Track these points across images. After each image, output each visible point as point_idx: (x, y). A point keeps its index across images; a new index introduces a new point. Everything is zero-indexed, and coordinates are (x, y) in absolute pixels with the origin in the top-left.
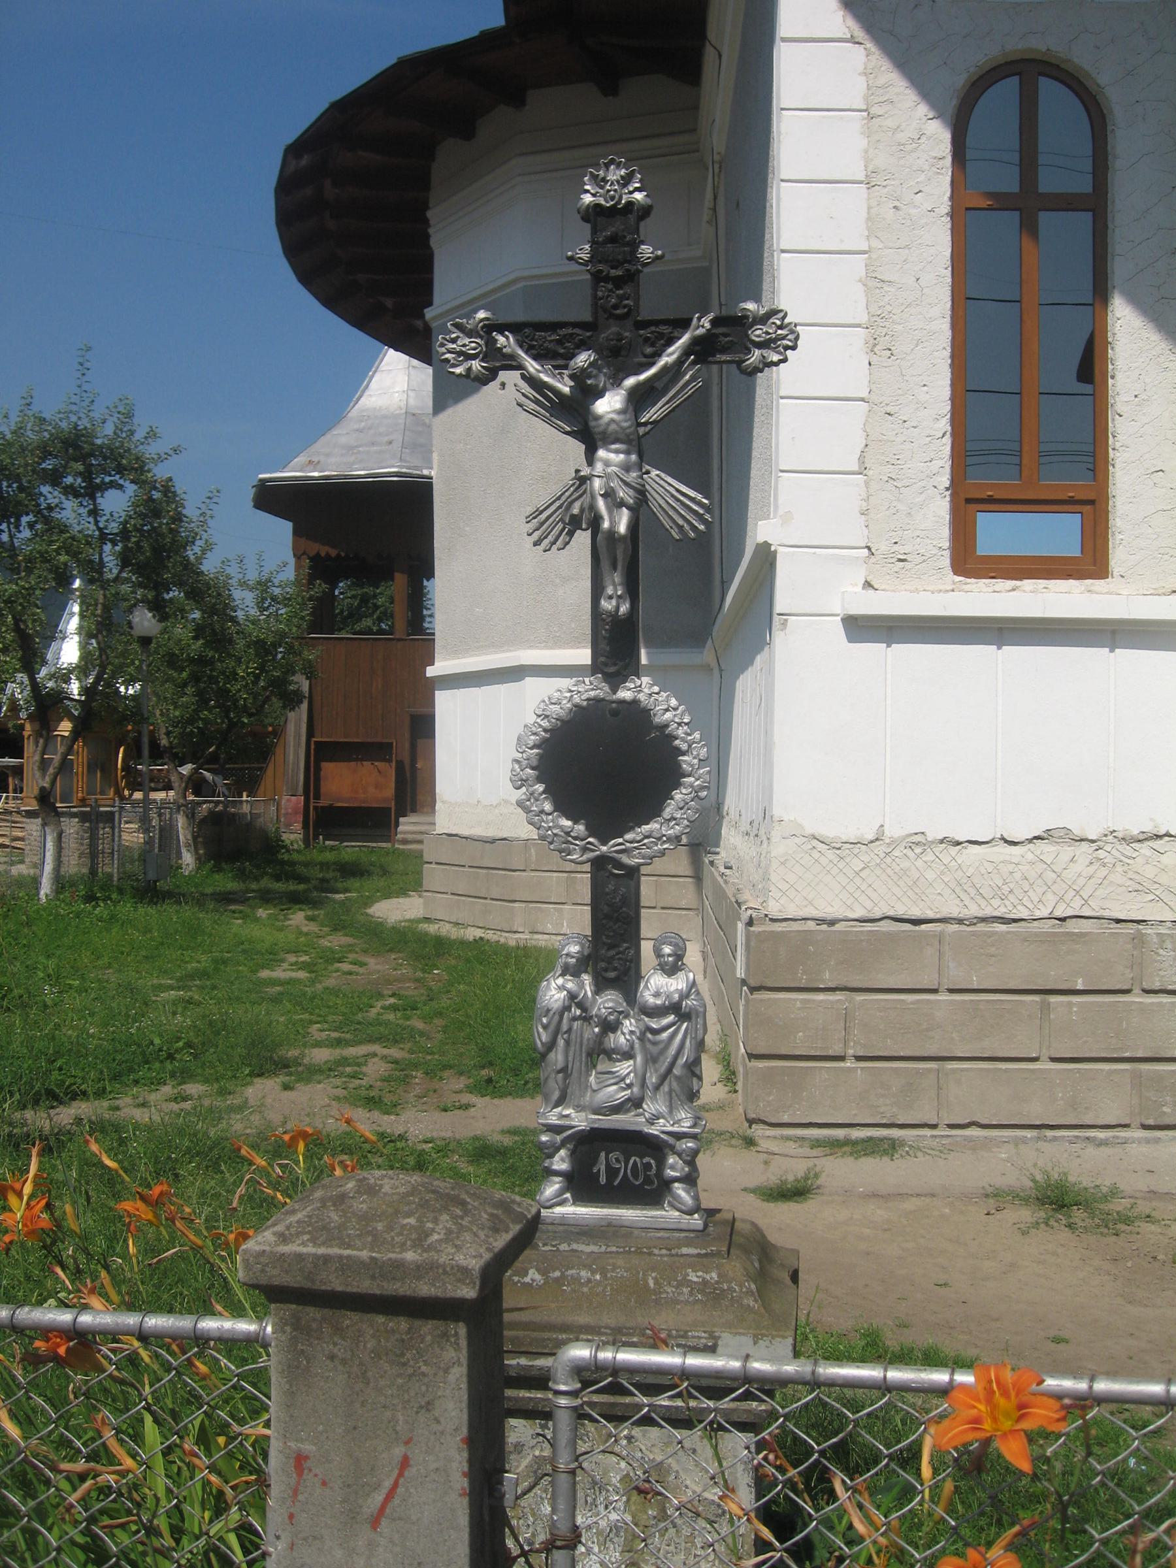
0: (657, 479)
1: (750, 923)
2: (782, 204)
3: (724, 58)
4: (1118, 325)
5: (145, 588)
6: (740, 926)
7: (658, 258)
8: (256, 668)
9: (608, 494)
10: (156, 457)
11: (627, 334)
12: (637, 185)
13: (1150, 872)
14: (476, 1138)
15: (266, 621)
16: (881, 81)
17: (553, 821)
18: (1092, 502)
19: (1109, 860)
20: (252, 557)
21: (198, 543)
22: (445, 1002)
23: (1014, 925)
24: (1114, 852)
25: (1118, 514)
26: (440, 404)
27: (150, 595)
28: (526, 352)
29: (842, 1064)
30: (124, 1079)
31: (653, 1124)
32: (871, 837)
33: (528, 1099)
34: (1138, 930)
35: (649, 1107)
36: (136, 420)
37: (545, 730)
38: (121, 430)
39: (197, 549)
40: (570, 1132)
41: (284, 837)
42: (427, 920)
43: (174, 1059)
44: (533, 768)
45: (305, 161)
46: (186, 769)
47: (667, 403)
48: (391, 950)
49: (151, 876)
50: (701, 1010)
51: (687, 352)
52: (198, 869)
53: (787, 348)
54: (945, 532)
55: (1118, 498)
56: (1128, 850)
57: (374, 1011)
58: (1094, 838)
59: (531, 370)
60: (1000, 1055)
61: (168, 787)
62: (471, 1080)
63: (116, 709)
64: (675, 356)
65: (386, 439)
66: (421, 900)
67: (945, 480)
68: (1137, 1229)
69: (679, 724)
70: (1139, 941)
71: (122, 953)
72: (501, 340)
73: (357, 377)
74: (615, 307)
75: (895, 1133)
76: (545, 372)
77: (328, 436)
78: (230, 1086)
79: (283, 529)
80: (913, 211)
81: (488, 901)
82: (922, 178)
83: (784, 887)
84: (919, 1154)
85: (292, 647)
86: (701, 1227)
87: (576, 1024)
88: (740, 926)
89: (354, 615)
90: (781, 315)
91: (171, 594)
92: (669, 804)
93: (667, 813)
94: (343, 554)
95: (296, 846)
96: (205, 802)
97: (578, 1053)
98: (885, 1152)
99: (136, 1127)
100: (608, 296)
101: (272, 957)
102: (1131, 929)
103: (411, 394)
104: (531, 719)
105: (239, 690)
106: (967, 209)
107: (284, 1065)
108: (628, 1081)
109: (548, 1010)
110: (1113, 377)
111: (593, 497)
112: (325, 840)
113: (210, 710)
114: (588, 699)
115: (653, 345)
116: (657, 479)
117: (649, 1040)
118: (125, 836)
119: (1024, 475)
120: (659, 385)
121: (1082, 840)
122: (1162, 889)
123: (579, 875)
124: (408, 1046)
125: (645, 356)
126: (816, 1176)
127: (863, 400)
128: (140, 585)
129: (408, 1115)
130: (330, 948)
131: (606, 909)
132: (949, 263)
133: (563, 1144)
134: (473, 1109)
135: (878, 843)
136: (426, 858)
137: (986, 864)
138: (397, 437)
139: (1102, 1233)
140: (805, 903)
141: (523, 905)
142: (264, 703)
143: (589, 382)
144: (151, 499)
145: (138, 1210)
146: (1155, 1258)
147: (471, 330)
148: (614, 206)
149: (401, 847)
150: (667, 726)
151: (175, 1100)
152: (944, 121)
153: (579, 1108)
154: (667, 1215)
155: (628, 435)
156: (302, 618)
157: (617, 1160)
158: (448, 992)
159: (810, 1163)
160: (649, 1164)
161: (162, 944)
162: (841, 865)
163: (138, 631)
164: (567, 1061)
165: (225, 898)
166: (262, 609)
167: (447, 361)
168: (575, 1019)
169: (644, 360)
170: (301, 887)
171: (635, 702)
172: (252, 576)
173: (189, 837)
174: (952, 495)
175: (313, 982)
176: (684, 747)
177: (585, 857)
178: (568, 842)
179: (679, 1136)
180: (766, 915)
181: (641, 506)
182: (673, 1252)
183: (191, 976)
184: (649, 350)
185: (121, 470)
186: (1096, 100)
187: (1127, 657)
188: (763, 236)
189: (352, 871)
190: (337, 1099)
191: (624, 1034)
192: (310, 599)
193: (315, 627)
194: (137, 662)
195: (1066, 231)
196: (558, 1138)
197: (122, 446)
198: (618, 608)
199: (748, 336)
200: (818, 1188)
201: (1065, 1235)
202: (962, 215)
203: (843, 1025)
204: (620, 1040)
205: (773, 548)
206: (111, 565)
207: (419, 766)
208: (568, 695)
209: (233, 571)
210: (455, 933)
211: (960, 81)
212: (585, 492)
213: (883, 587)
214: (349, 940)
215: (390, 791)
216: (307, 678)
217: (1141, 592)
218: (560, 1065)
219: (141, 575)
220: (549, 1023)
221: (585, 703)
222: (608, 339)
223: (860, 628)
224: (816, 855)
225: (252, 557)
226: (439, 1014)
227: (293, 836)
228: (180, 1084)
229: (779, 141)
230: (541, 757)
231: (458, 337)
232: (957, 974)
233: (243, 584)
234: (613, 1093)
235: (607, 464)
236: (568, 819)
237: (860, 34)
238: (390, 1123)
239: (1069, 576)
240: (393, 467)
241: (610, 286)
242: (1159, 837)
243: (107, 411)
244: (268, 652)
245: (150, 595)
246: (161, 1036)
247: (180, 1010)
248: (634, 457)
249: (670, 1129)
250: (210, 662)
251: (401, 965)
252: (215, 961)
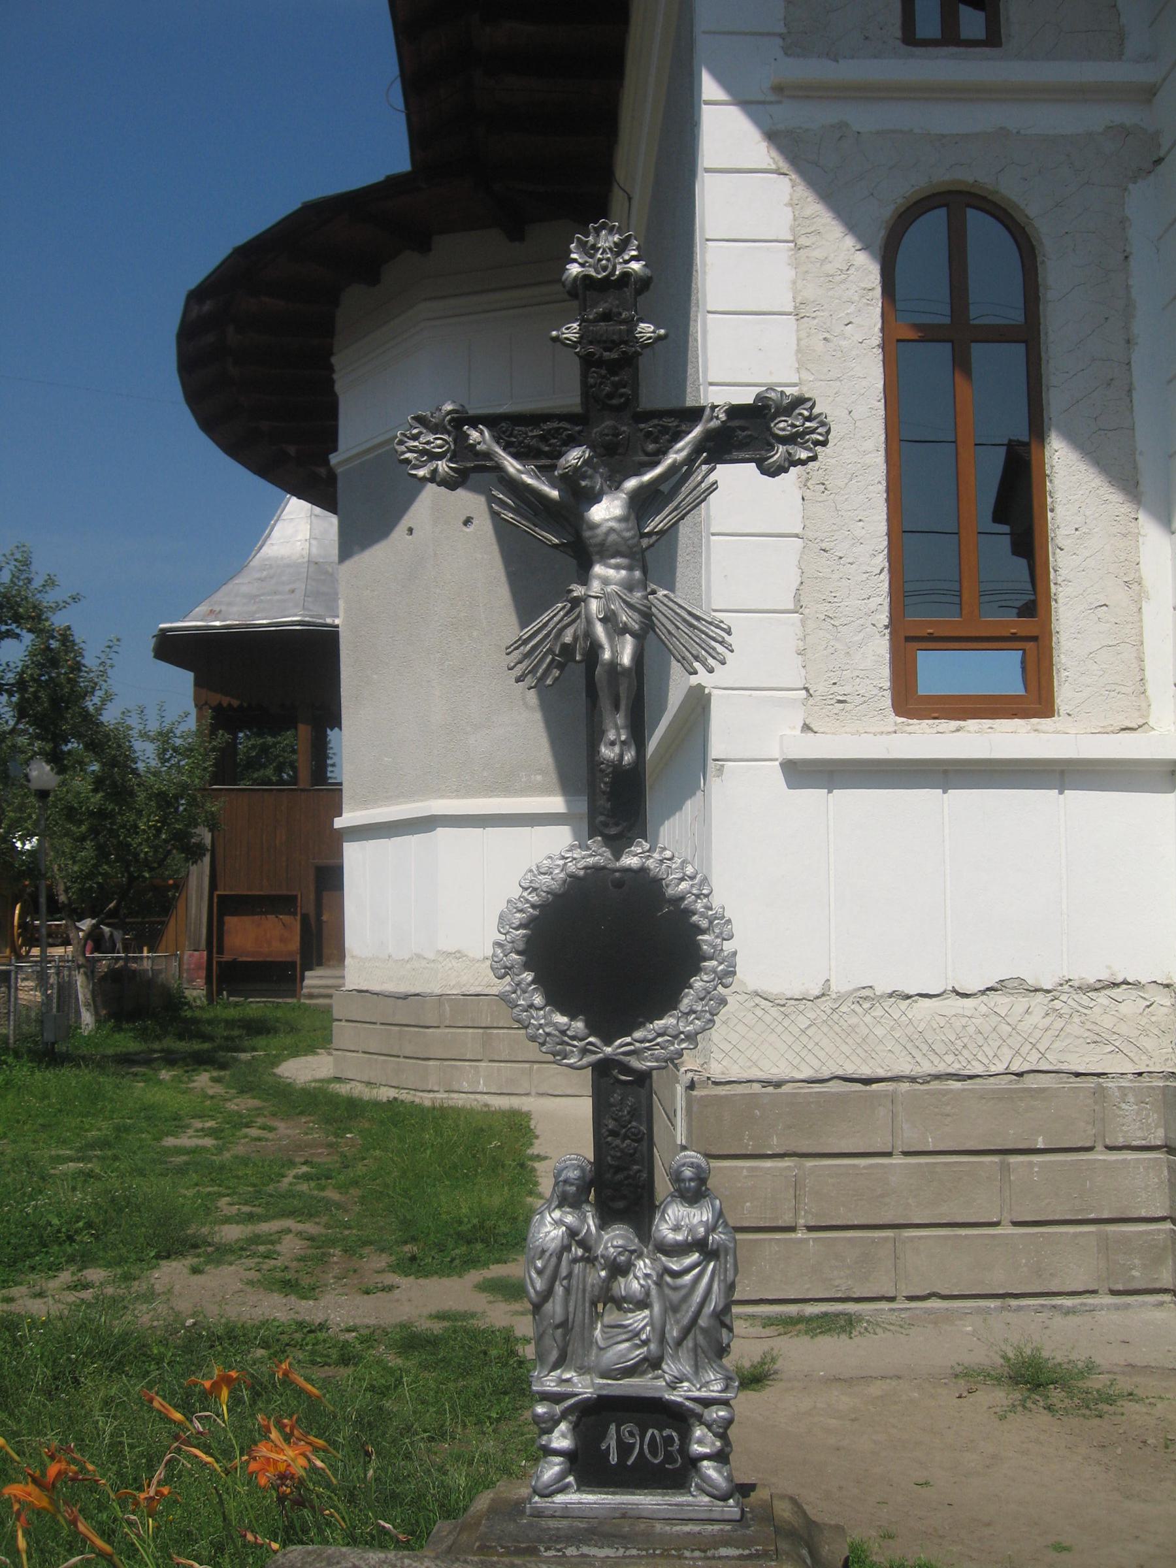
0: (666, 600)
1: (692, 1086)
2: (710, 337)
3: (635, 203)
4: (1056, 457)
5: (42, 740)
6: (680, 1089)
7: (660, 338)
8: (157, 821)
9: (609, 619)
10: (53, 605)
11: (624, 428)
12: (634, 253)
13: (1108, 1022)
14: (403, 1326)
15: (168, 773)
16: (808, 212)
17: (544, 1017)
18: (1035, 639)
19: (1065, 1010)
20: (148, 706)
21: (98, 693)
22: (360, 1169)
23: (969, 1081)
24: (1070, 1002)
25: (1063, 651)
26: (345, 553)
27: (48, 747)
28: (504, 450)
29: (793, 1235)
30: (19, 1265)
31: (674, 1388)
32: (817, 992)
33: (455, 1278)
34: (1099, 1084)
35: (670, 1368)
36: (33, 568)
37: (533, 906)
38: (18, 578)
39: (96, 700)
40: (572, 1401)
41: (187, 993)
42: (338, 1079)
43: (74, 1241)
44: (519, 953)
45: (207, 307)
46: (86, 924)
47: (675, 509)
48: (302, 1113)
49: (49, 1036)
50: (731, 1245)
51: (697, 449)
52: (98, 1028)
53: (817, 443)
54: (886, 672)
55: (1061, 633)
56: (1084, 1000)
57: (286, 1180)
58: (1049, 987)
59: (511, 470)
60: (959, 1220)
61: (66, 942)
62: (393, 1258)
63: (12, 865)
64: (684, 453)
65: (288, 588)
66: (331, 1058)
67: (883, 618)
68: (1120, 1410)
69: (698, 896)
70: (1100, 1094)
71: (18, 1122)
72: (474, 435)
73: (258, 527)
74: (610, 396)
75: (850, 1307)
76: (527, 473)
77: (230, 586)
78: (135, 1270)
79: (182, 681)
80: (844, 343)
81: (401, 1060)
82: (852, 309)
83: (727, 1047)
84: (879, 1330)
85: (195, 799)
86: (738, 1517)
87: (577, 1268)
88: (680, 1089)
89: (252, 764)
90: (809, 404)
91: (70, 746)
92: (687, 995)
93: (685, 1004)
94: (245, 705)
95: (198, 1003)
96: (105, 958)
97: (580, 1302)
98: (843, 1329)
99: (33, 1325)
100: (601, 384)
101: (177, 1123)
102: (1091, 1083)
103: (314, 542)
104: (517, 892)
105: (141, 844)
106: (898, 341)
107: (194, 1245)
108: (644, 1337)
109: (543, 1252)
110: (1052, 510)
111: (589, 622)
112: (229, 995)
113: (108, 863)
114: (586, 868)
115: (656, 441)
116: (666, 600)
117: (668, 1285)
118: (21, 995)
119: (964, 612)
120: (665, 488)
121: (1036, 990)
122: (1121, 1039)
123: (495, 1031)
124: (324, 1219)
125: (647, 454)
126: (773, 1360)
127: (797, 536)
128: (38, 737)
129: (328, 1299)
130: (237, 1112)
131: (611, 1124)
132: (882, 395)
133: (564, 1415)
134: (397, 1291)
135: (824, 999)
136: (336, 1015)
137: (938, 1018)
138: (301, 586)
139: (1084, 1416)
140: (749, 1064)
141: (438, 1063)
142: (166, 857)
143: (583, 483)
144: (48, 648)
145: (30, 1495)
146: (1145, 1442)
147: (436, 425)
148: (607, 278)
149: (307, 1001)
150: (683, 898)
151: (75, 1288)
152: (873, 255)
153: (582, 1370)
154: (695, 1500)
155: (630, 548)
156: (205, 769)
157: (631, 1434)
158: (364, 1159)
159: (765, 1345)
160: (671, 1437)
161: (60, 1111)
162: (786, 1023)
163: (34, 785)
164: (567, 1313)
165: (126, 1059)
166: (164, 761)
167: (407, 461)
168: (575, 1260)
169: (646, 458)
170: (208, 1047)
171: (643, 870)
172: (153, 727)
173: (89, 996)
174: (891, 633)
175: (220, 1150)
176: (704, 924)
177: (585, 1061)
178: (563, 1043)
179: (707, 1403)
180: (709, 1078)
181: (647, 633)
182: (709, 1553)
183: (92, 1146)
184: (651, 447)
185: (17, 619)
186: (1025, 232)
187: (1076, 798)
188: (686, 371)
189: (258, 1028)
190: (251, 1283)
191: (637, 1278)
192: (214, 749)
193: (216, 778)
194: (34, 816)
195: (998, 362)
196: (558, 1409)
197: (19, 594)
198: (621, 756)
199: (769, 429)
200: (776, 1372)
201: (1045, 1418)
202: (894, 347)
203: (792, 1191)
204: (633, 1285)
205: (707, 691)
206: (7, 716)
207: (324, 918)
208: (561, 862)
209: (133, 721)
210: (367, 1094)
211: (887, 212)
212: (578, 616)
213: (822, 730)
214: (257, 1103)
215: (295, 944)
216: (211, 830)
217: (1089, 730)
218: (559, 1318)
219: (39, 727)
220: (545, 1267)
221: (582, 873)
222: (602, 435)
223: (803, 773)
224: (759, 1012)
225: (148, 706)
226: (355, 1183)
227: (196, 992)
228: (80, 1270)
229: (704, 273)
230: (529, 940)
231: (420, 433)
232: (911, 1137)
233: (144, 736)
234: (622, 1351)
235: (606, 581)
236: (563, 1014)
237: (784, 166)
238: (308, 1310)
239: (1013, 715)
240: (296, 615)
241: (603, 372)
242: (1116, 985)
243: (3, 559)
244: (169, 804)
245: (48, 747)
246: (59, 1215)
247: (80, 1185)
248: (637, 574)
249: (697, 1394)
250: (111, 815)
251: (312, 1129)
252: (118, 1129)
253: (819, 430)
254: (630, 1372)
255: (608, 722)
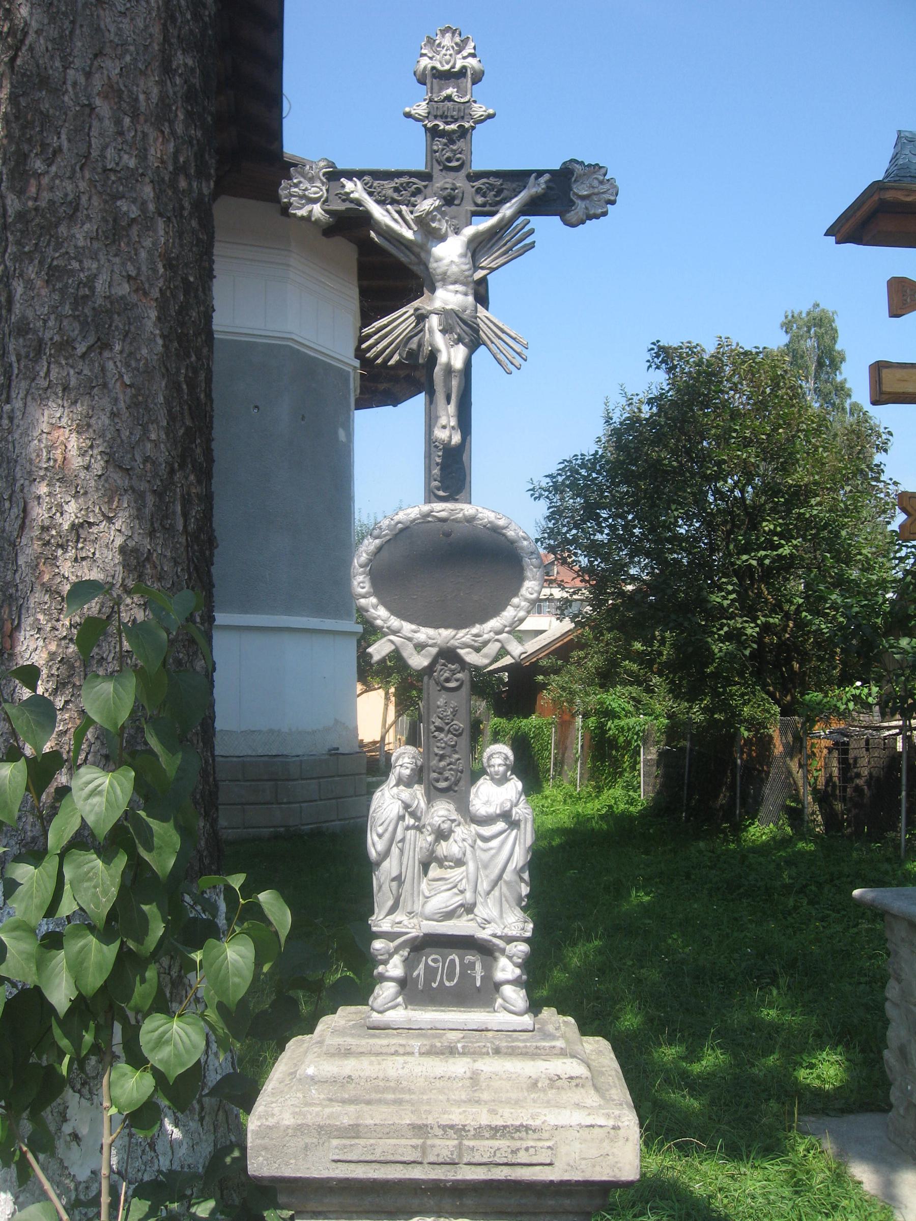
90: (603, 171)
133: (397, 950)
168: (408, 828)
196: (392, 945)
218: (395, 873)
231: (300, 182)
234: (442, 900)
253: (610, 191)
254: (449, 915)
255: (441, 412)
